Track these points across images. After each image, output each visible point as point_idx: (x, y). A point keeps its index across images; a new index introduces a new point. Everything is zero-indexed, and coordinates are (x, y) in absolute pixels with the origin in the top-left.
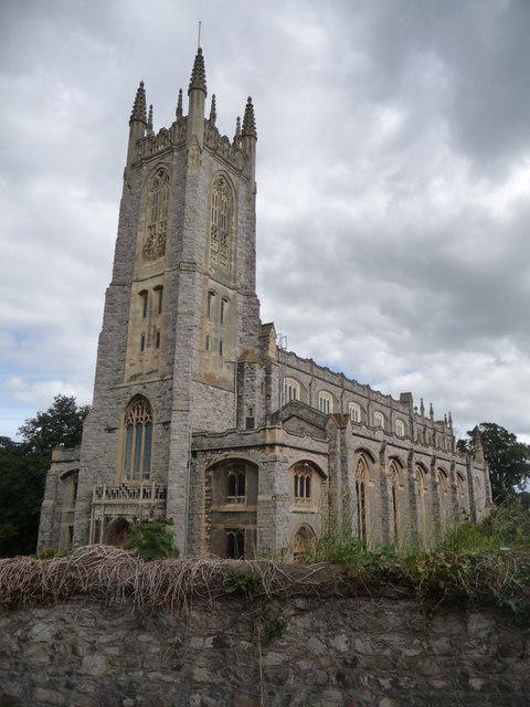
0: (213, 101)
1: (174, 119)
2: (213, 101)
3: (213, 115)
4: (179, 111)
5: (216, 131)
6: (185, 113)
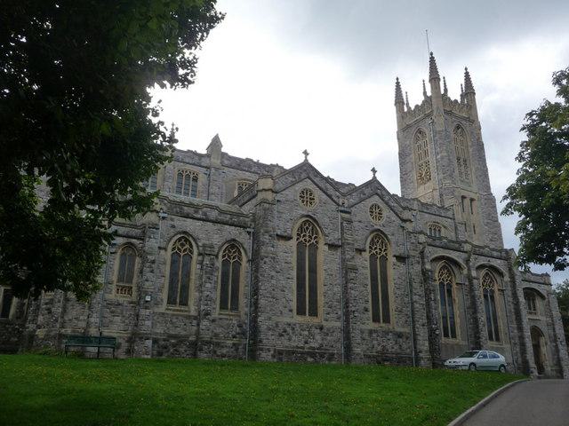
0: (445, 84)
1: (423, 98)
2: (445, 84)
3: (446, 90)
4: (425, 93)
5: (449, 99)
6: (429, 94)
